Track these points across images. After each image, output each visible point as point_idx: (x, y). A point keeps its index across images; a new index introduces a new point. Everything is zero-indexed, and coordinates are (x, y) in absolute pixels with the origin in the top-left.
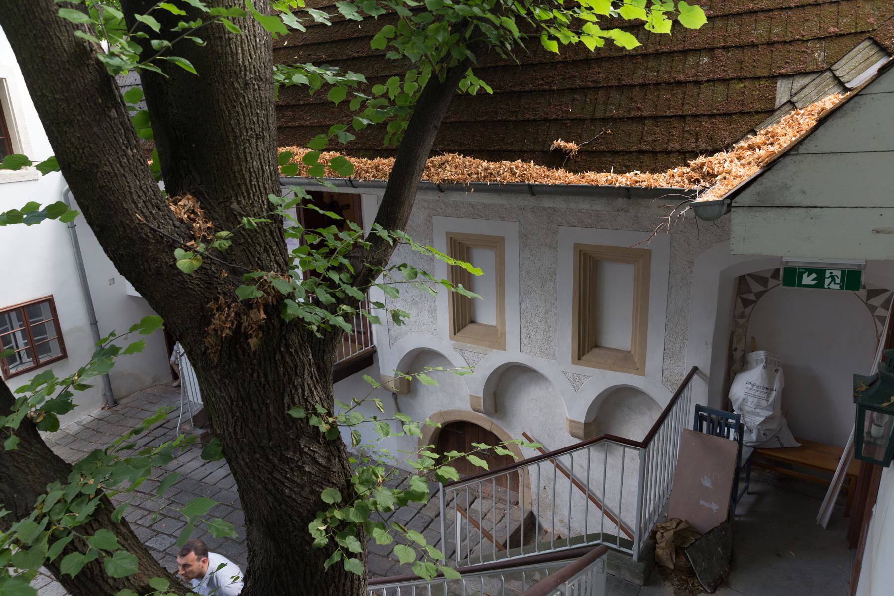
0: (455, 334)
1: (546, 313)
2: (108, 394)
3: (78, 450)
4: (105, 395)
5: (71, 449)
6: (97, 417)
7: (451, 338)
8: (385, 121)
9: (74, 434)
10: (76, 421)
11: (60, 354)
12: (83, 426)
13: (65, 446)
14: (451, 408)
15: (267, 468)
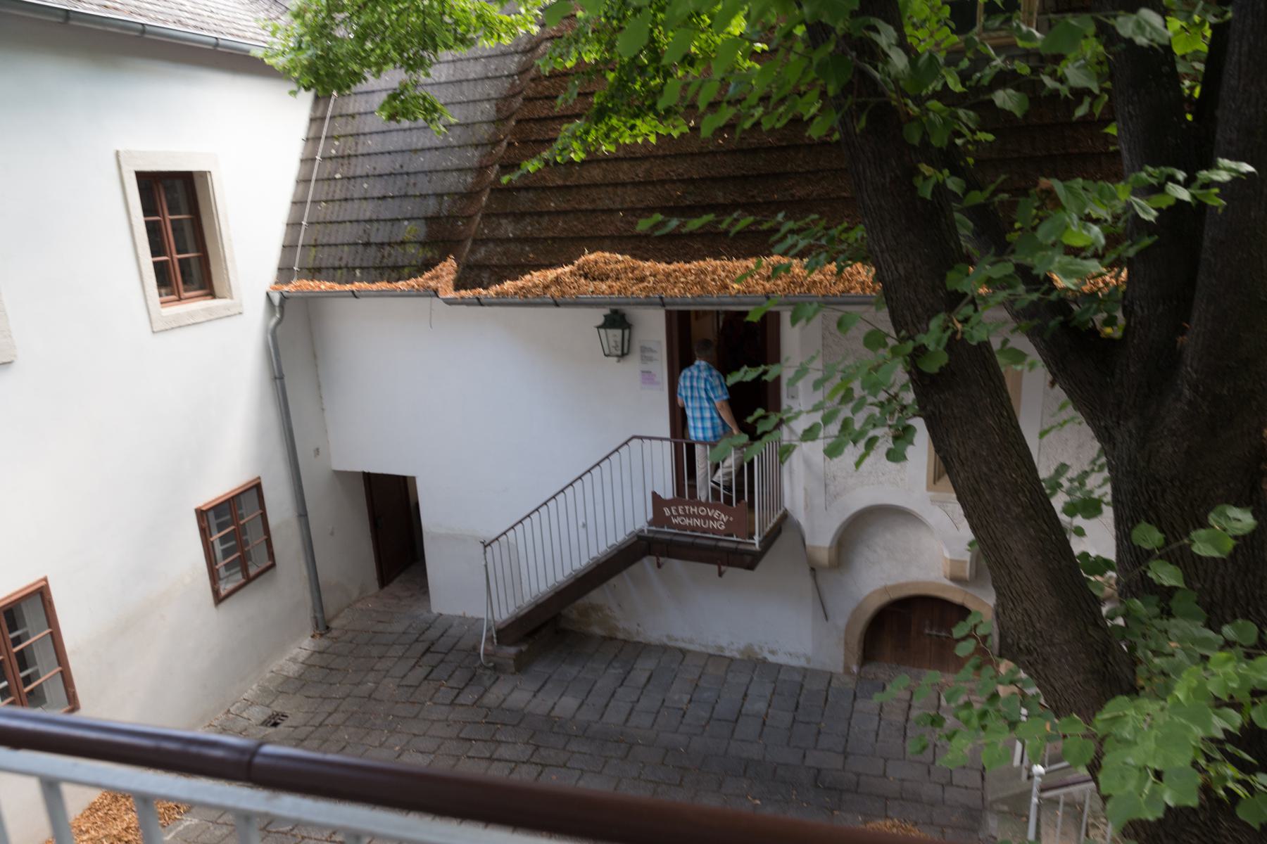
0: (935, 483)
1: (1080, 446)
2: (318, 615)
3: (321, 697)
4: (315, 617)
5: (308, 697)
6: (312, 649)
7: (929, 489)
8: (731, 119)
9: (296, 675)
10: (287, 658)
11: (270, 563)
12: (303, 663)
13: (295, 694)
14: (902, 580)
15: (338, 191)
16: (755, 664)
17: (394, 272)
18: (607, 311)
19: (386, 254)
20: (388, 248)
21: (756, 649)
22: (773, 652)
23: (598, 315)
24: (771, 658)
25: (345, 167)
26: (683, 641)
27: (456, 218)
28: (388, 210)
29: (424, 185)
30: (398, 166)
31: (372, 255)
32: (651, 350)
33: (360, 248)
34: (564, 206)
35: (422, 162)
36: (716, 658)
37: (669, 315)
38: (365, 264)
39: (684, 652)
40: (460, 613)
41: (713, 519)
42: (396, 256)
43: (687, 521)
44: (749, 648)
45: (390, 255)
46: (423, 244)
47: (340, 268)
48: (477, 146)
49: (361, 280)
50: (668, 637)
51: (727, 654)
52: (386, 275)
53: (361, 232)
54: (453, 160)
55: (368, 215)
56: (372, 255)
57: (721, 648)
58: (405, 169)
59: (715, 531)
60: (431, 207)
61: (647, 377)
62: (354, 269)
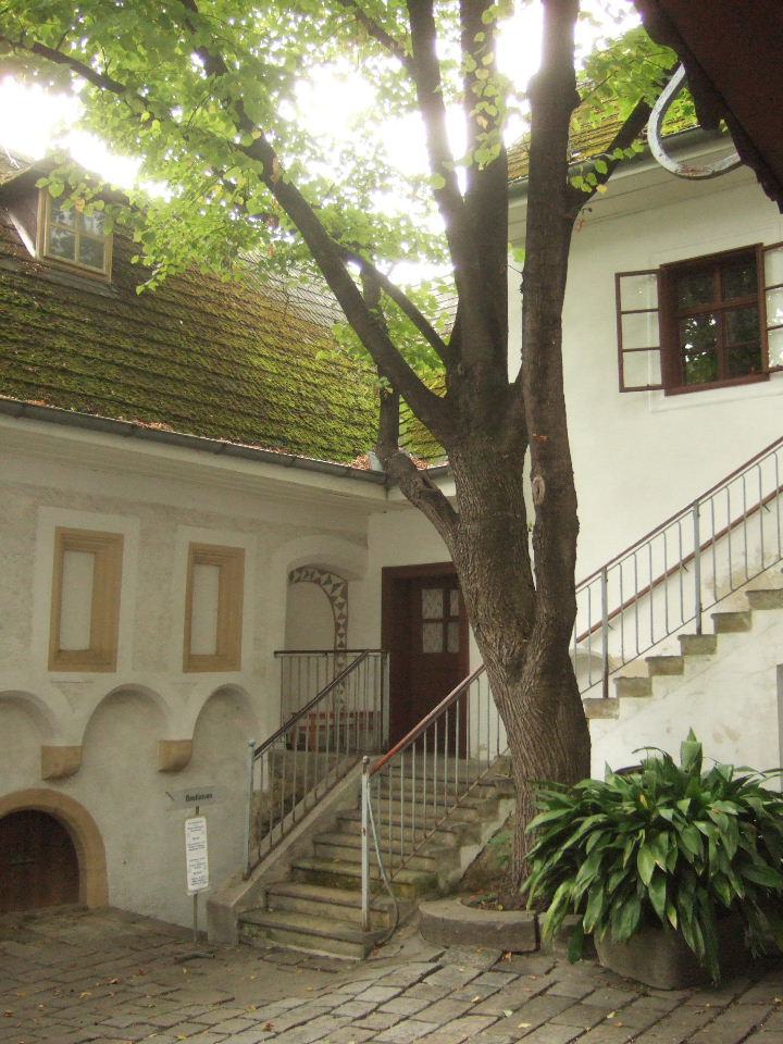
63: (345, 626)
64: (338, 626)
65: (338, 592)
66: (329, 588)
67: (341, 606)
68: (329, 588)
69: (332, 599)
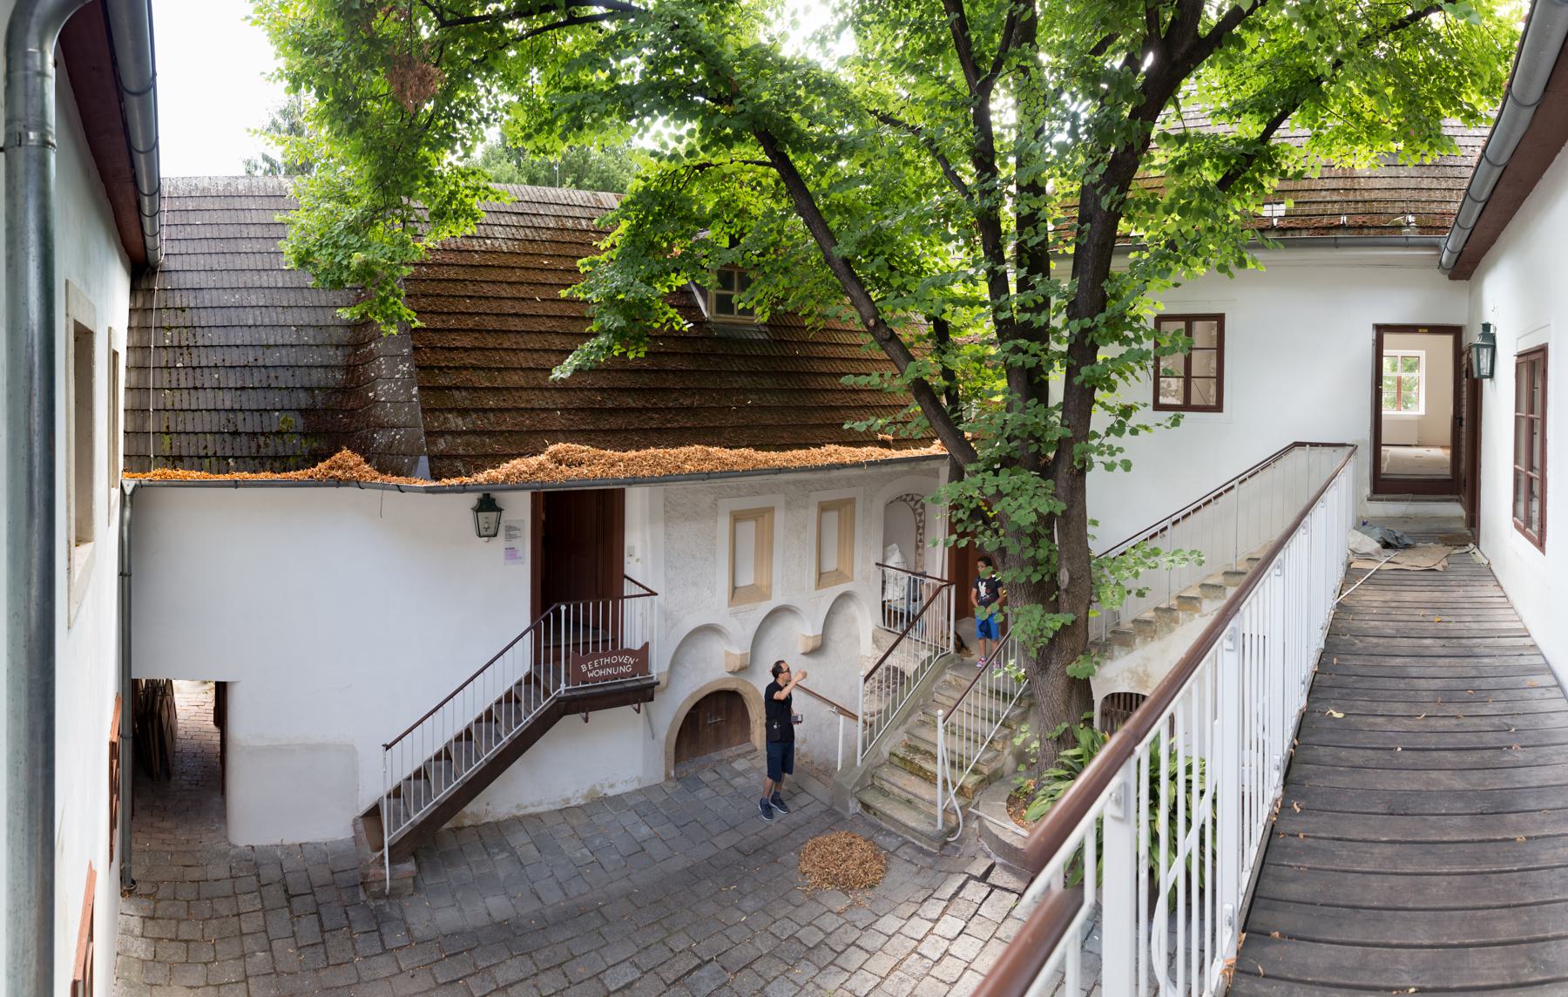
16: (599, 803)
17: (281, 463)
18: (480, 495)
19: (262, 443)
20: (262, 440)
21: (598, 788)
22: (612, 786)
23: (472, 499)
24: (611, 793)
25: (186, 357)
26: (533, 805)
27: (335, 412)
28: (252, 401)
29: (285, 379)
30: (251, 359)
31: (243, 446)
32: (515, 529)
33: (227, 437)
34: (502, 404)
35: (274, 357)
36: (565, 812)
37: (535, 497)
38: (238, 454)
39: (538, 816)
40: (278, 842)
41: (622, 664)
42: (273, 446)
43: (601, 673)
44: (592, 790)
45: (266, 445)
46: (304, 435)
47: (207, 456)
48: (337, 347)
49: (237, 470)
50: (518, 806)
51: (573, 803)
52: (268, 466)
53: (223, 421)
54: (315, 358)
55: (228, 405)
56: (243, 446)
57: (567, 800)
58: (260, 363)
59: (623, 675)
60: (303, 400)
61: (511, 553)
62: (226, 458)
63: (923, 527)
64: (918, 528)
65: (918, 506)
66: (912, 503)
67: (920, 515)
68: (912, 503)
69: (914, 510)
